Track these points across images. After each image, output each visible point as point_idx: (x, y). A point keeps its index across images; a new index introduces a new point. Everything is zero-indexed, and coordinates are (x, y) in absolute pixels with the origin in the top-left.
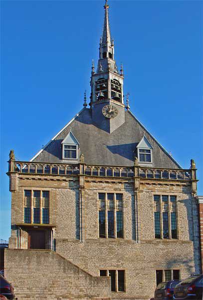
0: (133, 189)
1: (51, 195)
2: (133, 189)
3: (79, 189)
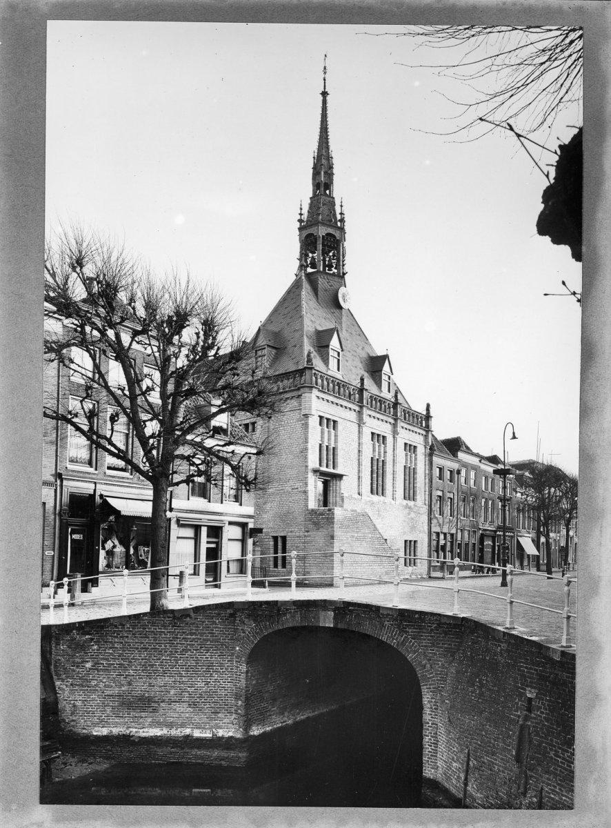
0: (395, 433)
1: (340, 427)
2: (395, 433)
3: (360, 423)
